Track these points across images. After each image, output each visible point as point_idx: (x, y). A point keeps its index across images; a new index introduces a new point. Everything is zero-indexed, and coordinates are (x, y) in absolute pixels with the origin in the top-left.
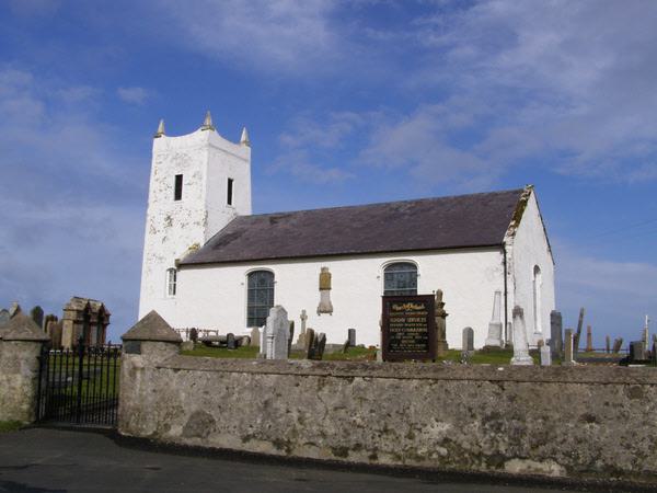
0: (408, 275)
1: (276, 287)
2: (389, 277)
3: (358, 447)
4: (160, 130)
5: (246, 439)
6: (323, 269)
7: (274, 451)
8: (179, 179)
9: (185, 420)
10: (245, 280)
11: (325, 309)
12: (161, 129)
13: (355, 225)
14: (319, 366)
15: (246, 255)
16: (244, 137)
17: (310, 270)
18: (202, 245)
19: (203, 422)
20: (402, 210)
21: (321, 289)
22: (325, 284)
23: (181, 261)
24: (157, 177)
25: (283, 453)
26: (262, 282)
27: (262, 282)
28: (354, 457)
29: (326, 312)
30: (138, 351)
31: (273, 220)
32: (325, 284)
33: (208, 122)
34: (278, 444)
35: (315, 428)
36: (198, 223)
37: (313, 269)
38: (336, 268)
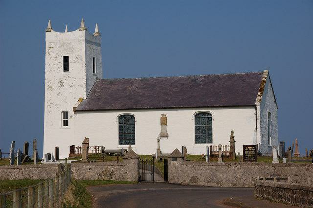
0: (207, 119)
1: (136, 124)
2: (197, 119)
3: (239, 183)
4: (49, 26)
5: (209, 182)
6: (163, 115)
7: (216, 185)
8: (66, 59)
9: (190, 179)
10: (117, 119)
11: (164, 135)
12: (49, 26)
13: (174, 90)
14: (227, 163)
15: (118, 106)
16: (82, 25)
17: (155, 116)
18: (85, 98)
19: (194, 179)
20: (198, 81)
21: (161, 125)
22: (164, 122)
23: (77, 109)
24: (51, 56)
25: (219, 185)
26: (127, 120)
27: (127, 120)
28: (238, 186)
29: (165, 137)
30: (176, 160)
31: (112, 83)
32: (164, 122)
33: (82, 25)
34: (218, 183)
35: (227, 179)
36: (81, 86)
37: (157, 115)
38: (171, 114)
